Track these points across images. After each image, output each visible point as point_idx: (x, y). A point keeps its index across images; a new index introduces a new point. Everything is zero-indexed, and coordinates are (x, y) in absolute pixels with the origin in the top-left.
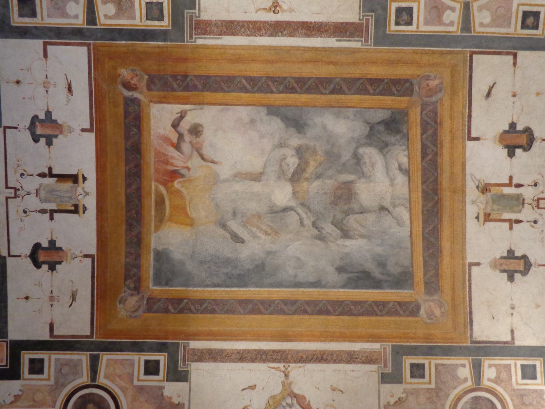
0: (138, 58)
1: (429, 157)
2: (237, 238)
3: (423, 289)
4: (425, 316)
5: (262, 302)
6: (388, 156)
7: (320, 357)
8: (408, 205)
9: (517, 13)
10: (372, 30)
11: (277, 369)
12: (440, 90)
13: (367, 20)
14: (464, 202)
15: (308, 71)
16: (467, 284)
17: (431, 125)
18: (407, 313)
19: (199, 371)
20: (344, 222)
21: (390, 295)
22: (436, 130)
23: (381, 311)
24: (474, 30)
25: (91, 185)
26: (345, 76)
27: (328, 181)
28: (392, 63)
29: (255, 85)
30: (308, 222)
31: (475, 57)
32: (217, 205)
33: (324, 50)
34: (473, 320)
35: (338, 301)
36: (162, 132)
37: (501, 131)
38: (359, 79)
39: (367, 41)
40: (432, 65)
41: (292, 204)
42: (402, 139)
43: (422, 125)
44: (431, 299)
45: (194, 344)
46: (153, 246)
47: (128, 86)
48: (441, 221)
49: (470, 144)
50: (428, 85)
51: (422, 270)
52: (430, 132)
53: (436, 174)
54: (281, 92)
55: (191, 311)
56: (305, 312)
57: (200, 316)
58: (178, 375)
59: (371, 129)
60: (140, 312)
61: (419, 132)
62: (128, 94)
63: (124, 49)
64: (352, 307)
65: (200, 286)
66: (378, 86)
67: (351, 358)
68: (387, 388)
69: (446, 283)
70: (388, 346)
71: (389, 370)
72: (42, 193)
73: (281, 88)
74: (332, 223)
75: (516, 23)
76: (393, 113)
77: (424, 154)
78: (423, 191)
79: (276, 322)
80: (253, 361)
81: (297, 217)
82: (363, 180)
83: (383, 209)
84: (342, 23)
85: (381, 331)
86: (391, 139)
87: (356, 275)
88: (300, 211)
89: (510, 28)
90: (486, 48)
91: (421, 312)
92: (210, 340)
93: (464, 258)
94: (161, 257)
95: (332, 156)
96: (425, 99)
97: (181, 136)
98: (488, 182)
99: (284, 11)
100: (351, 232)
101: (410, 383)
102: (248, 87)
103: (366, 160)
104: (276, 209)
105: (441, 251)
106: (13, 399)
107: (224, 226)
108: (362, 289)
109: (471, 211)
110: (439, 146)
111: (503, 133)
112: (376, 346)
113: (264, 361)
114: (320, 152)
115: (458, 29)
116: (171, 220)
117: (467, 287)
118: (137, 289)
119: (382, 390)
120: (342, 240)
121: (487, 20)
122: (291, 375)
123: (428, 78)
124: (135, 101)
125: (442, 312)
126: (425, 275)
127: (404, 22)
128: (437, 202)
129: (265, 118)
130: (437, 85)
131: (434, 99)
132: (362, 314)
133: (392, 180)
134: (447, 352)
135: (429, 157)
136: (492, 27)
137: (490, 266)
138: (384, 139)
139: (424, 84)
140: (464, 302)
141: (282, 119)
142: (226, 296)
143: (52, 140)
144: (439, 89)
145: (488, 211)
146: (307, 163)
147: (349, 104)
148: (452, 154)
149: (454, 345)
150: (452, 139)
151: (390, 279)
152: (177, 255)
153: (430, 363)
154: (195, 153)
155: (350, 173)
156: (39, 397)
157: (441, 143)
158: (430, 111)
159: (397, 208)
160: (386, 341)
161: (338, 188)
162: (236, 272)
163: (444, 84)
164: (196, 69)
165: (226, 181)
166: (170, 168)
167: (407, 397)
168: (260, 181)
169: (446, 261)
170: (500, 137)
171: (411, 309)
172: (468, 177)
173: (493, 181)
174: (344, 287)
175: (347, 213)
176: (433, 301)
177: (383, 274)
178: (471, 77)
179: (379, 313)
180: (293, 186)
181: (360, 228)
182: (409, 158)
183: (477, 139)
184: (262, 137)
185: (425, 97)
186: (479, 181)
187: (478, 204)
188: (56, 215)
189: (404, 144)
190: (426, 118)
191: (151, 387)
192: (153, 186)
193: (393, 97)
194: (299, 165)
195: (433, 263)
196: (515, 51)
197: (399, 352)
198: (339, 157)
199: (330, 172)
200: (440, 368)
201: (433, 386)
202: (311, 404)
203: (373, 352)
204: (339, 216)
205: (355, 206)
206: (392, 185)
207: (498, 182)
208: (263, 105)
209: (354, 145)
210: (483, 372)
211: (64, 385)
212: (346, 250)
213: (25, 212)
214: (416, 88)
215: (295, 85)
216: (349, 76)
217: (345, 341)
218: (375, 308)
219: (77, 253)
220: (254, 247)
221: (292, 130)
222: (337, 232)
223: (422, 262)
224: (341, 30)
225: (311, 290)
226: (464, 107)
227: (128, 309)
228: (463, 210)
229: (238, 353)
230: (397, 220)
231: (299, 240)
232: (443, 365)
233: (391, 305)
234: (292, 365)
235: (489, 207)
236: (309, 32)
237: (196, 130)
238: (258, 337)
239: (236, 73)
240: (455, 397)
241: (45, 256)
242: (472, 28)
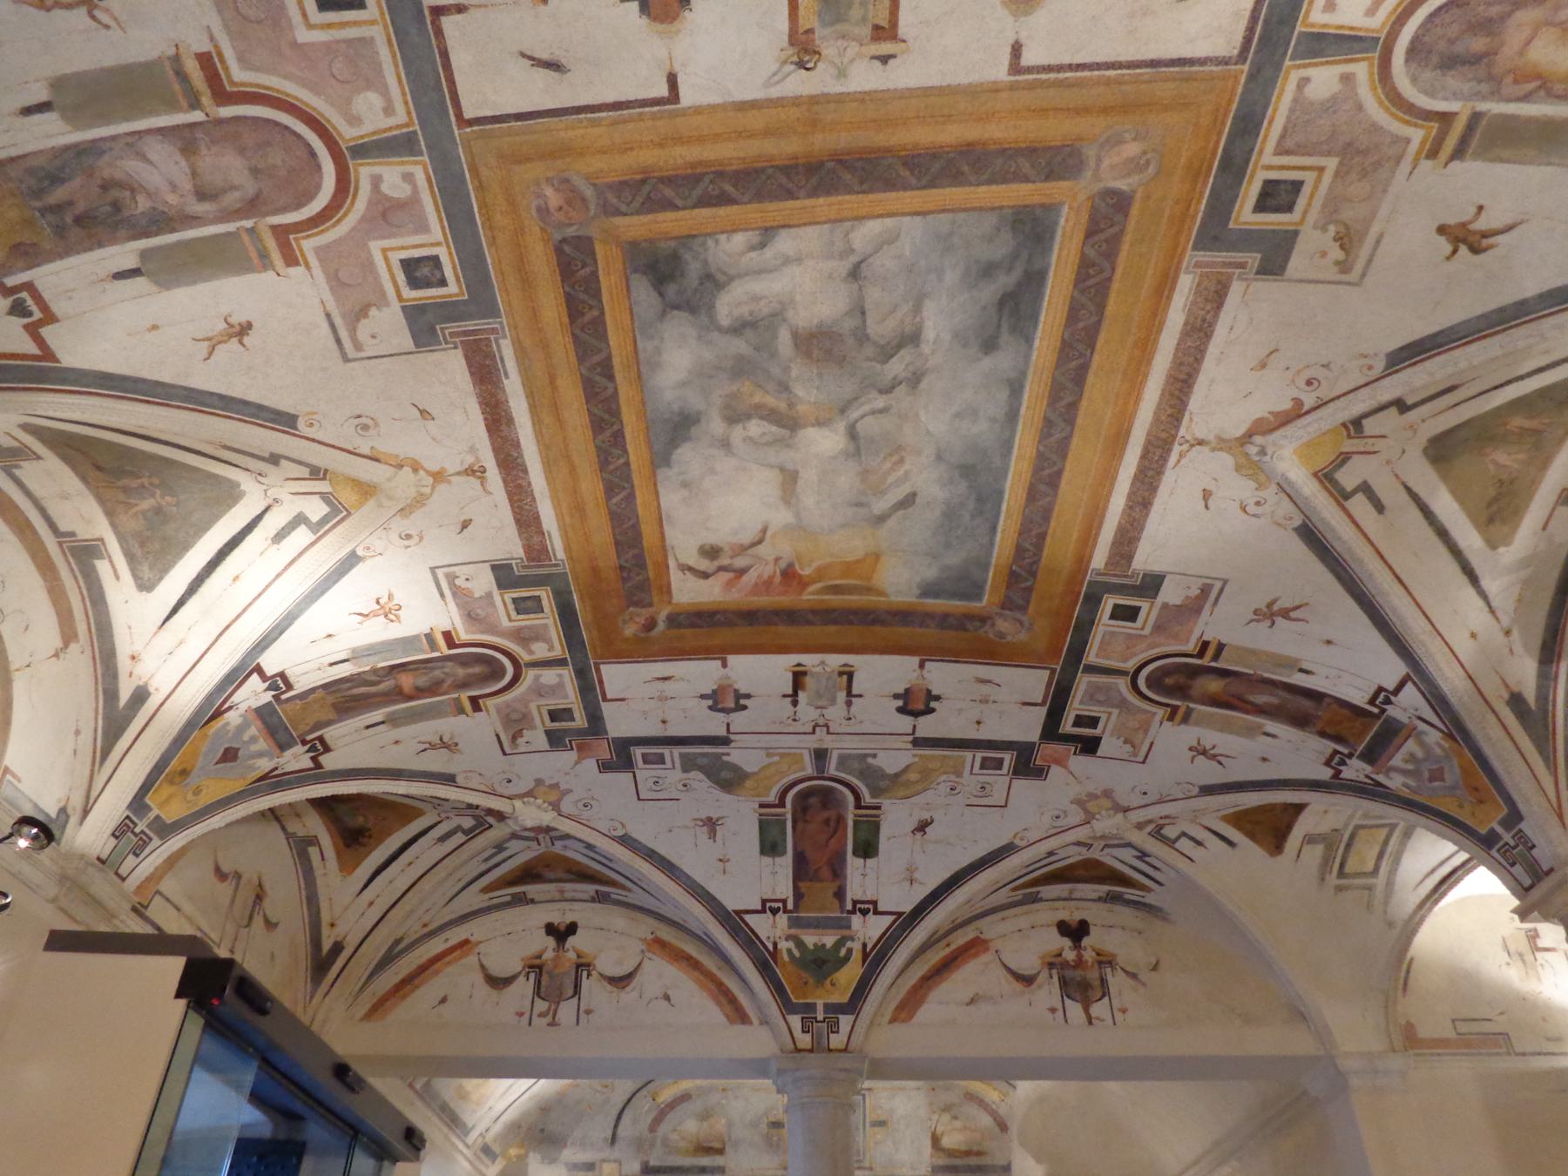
1: (729, 188)
2: (909, 501)
3: (1064, 184)
4: (1134, 180)
5: (1037, 469)
6: (733, 272)
7: (1178, 385)
8: (848, 224)
9: (330, 26)
10: (470, 325)
12: (567, 181)
13: (452, 335)
14: (840, 99)
16: (1068, 75)
17: (649, 191)
18: (1106, 265)
19: (1145, 559)
20: (882, 342)
21: (1065, 252)
22: (662, 180)
23: (1102, 271)
24: (407, 125)
25: (809, 660)
26: (573, 359)
27: (794, 373)
28: (527, 282)
29: (617, 481)
30: (880, 402)
31: (469, 114)
32: (843, 526)
34: (1175, 56)
35: (1062, 350)
36: (717, 590)
37: (645, 21)
38: (575, 337)
39: (494, 331)
40: (511, 201)
41: (841, 426)
42: (691, 249)
43: (650, 211)
44: (1092, 164)
45: (1099, 560)
46: (914, 600)
48: (888, 150)
49: (687, 97)
50: (560, 208)
51: (1014, 186)
52: (668, 192)
53: (770, 171)
54: (625, 451)
56: (1073, 406)
57: (1046, 552)
58: (1151, 584)
59: (677, 307)
60: (1024, 619)
61: (670, 215)
62: (661, 626)
63: (595, 633)
64: (1081, 325)
66: (583, 302)
67: (1199, 332)
68: (1297, 264)
69: (1054, 130)
70: (1190, 257)
71: (1253, 259)
73: (616, 452)
74: (885, 362)
75: (355, 23)
76: (636, 271)
77: (724, 200)
78: (814, 193)
79: (1083, 453)
80: (1153, 489)
81: (869, 420)
82: (790, 314)
83: (855, 274)
84: (472, 374)
85: (1150, 272)
86: (693, 269)
87: (1005, 319)
88: (855, 415)
89: (372, 39)
90: (441, 90)
91: (1124, 188)
92: (1095, 545)
93: (995, 89)
95: (740, 368)
96: (592, 212)
97: (721, 569)
98: (786, 38)
99: (478, 460)
100: (907, 330)
101: (1306, 213)
102: (624, 494)
103: (744, 311)
104: (852, 448)
105: (969, 144)
107: (881, 519)
108: (1040, 308)
109: (865, 77)
110: (698, 170)
111: (649, 15)
112: (1186, 283)
113: (1160, 473)
114: (734, 388)
115: (416, 163)
116: (869, 579)
117: (1079, 74)
118: (983, 619)
119: (1297, 276)
120: (922, 346)
121: (374, 98)
122: (1200, 435)
123: (543, 211)
124: (673, 620)
125: (1134, 139)
126: (1027, 180)
127: (437, 273)
128: (840, 161)
129: (675, 470)
130: (557, 190)
131: (589, 192)
132: (1101, 307)
133: (787, 261)
134: (1248, 125)
135: (729, 188)
136: (386, 86)
137: (1026, 14)
138: (696, 283)
139: (560, 216)
140: (1119, 81)
141: (676, 447)
142: (1016, 519)
144: (564, 184)
145: (866, 31)
146: (759, 407)
147: (630, 348)
148: (716, 137)
149: (1234, 106)
150: (679, 140)
151: (1025, 255)
152: (931, 573)
153: (1267, 162)
154: (750, 552)
155: (775, 337)
157: (693, 165)
158: (619, 197)
159: (855, 246)
160: (1180, 262)
161: (808, 355)
162: (971, 504)
163: (550, 174)
164: (608, 559)
165: (797, 515)
166: (778, 579)
167: (1337, 222)
168: (797, 472)
169: (997, 132)
170: (662, 22)
171: (1110, 212)
172: (775, 92)
173: (784, 25)
174: (1029, 340)
175: (862, 337)
176: (1099, 160)
177: (1010, 270)
178: (519, 117)
179: (1106, 275)
180: (805, 426)
181: (899, 315)
182: (734, 231)
183: (672, 81)
184: (712, 471)
185: (588, 209)
186: (785, 62)
187: (846, 60)
188: (855, 691)
189: (704, 244)
190: (636, 204)
192: (810, 597)
193: (601, 272)
194: (762, 418)
195: (999, 161)
196: (427, 12)
197: (1216, 232)
198: (740, 358)
199: (776, 371)
200: (1289, 143)
201: (1331, 163)
202: (1278, 409)
203: (1198, 290)
204: (869, 351)
205: (849, 324)
206: (799, 260)
207: (786, 12)
208: (654, 475)
209: (715, 335)
210: (1341, 27)
212: (947, 337)
214: (571, 231)
215: (608, 433)
216: (572, 354)
217: (1156, 341)
218: (1091, 282)
220: (927, 480)
222: (905, 355)
223: (994, 187)
224: (484, 373)
225: (1026, 396)
226: (595, 123)
228: (862, 98)
229: (1131, 508)
230: (883, 243)
231: (917, 415)
232: (1283, 137)
233: (1091, 253)
234: (1182, 432)
235: (857, 31)
236: (504, 421)
237: (711, 552)
238: (1108, 478)
239: (604, 511)
240: (1387, 110)
241: (915, 703)
242: (405, 130)
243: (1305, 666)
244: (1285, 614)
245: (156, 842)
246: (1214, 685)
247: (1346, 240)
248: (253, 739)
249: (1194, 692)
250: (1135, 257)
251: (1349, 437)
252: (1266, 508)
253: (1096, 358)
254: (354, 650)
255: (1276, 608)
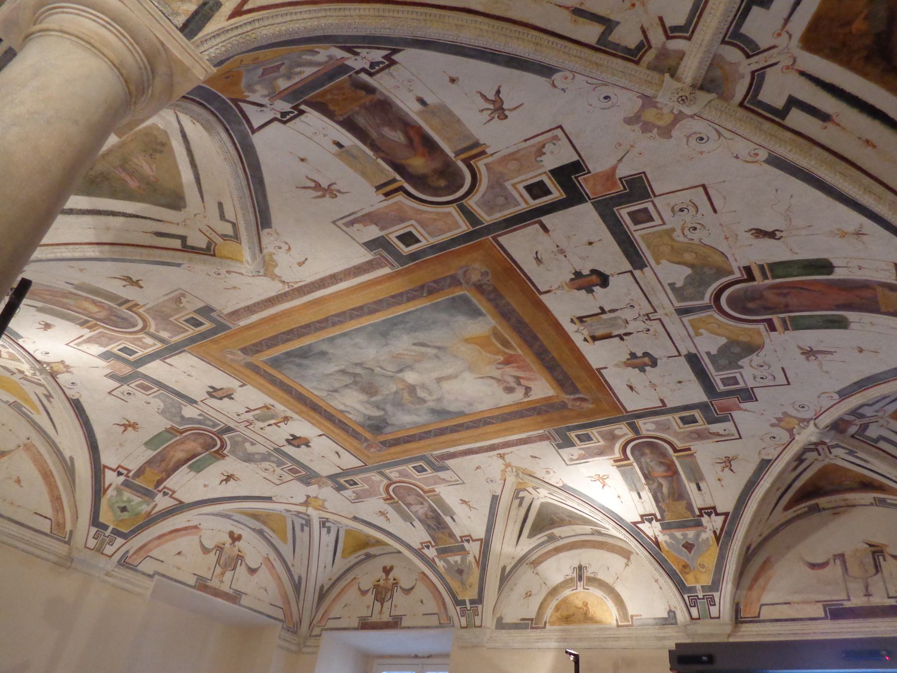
0: (581, 415)
11: (297, 282)
15: (456, 436)
30: (377, 370)
33: (453, 446)
45: (386, 270)
46: (489, 317)
47: (583, 400)
55: (413, 290)
58: (371, 245)
60: (460, 272)
65: (422, 308)
67: (250, 310)
68: (200, 305)
69: (248, 372)
72: (620, 322)
79: (333, 308)
83: (336, 391)
94: (475, 313)
106: (544, 150)
112: (243, 323)
143: (742, 34)
153: (192, 331)
156: (513, 165)
174: (310, 345)
191: (394, 225)
201: (171, 319)
204: (358, 379)
211: (491, 187)
213: (632, 306)
219: (559, 292)
220: (403, 343)
221: (438, 408)
227: (477, 268)
234: (287, 289)
243: (335, 149)
244: (318, 186)
245: (716, 595)
246: (418, 163)
247: (178, 300)
248: (685, 536)
249: (436, 164)
250: (254, 338)
251: (216, 244)
252: (278, 243)
253: (294, 326)
254: (631, 490)
255: (320, 193)
